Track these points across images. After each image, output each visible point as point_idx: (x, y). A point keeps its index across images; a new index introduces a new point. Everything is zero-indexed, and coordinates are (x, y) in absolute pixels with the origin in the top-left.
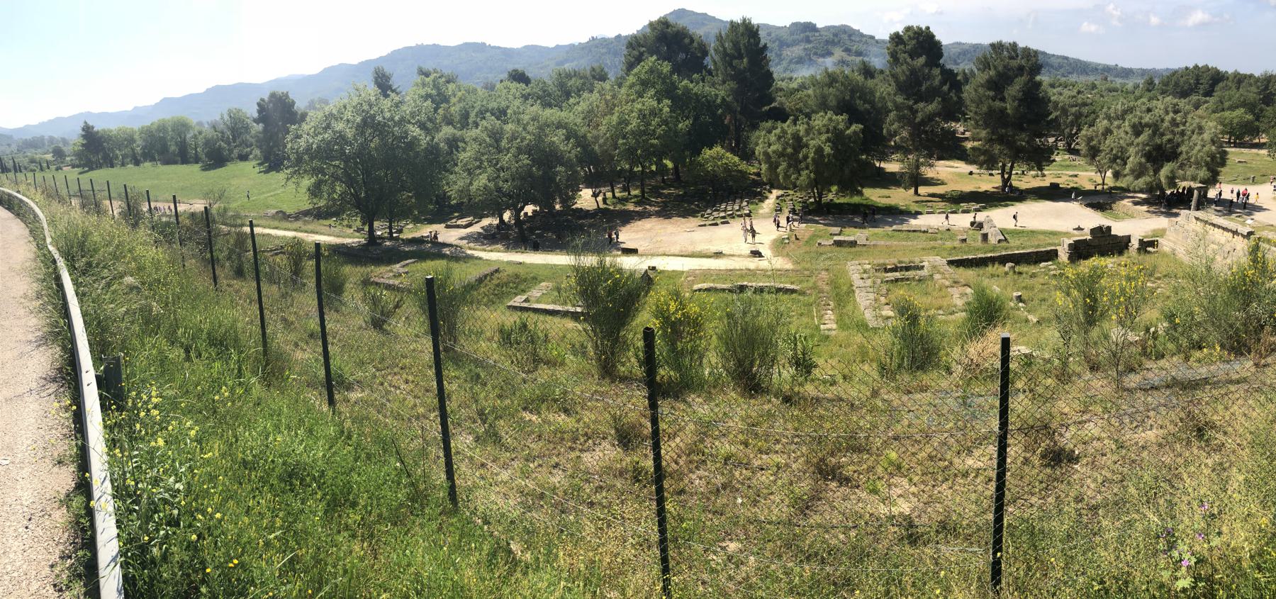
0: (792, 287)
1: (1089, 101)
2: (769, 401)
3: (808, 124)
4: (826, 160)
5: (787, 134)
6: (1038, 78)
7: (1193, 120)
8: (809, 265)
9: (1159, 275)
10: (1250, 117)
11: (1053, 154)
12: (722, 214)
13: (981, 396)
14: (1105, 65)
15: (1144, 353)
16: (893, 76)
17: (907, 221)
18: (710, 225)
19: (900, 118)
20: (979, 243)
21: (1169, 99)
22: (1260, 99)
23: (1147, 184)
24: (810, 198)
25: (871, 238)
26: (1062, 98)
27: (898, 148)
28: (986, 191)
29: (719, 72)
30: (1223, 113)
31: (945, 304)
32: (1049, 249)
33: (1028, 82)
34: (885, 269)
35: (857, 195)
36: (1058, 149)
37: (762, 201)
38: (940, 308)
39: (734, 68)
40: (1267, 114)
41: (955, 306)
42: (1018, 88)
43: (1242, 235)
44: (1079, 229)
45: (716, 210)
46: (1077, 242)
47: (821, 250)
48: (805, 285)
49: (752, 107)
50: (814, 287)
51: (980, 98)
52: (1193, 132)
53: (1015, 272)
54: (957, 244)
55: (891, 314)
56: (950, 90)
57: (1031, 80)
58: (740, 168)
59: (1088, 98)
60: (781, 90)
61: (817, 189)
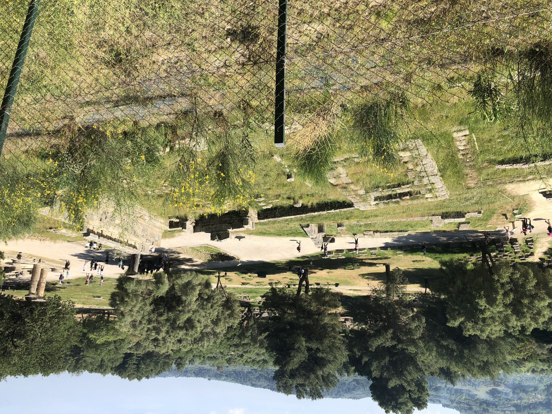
0: (504, 167)
1: (233, 349)
3: (508, 327)
4: (482, 293)
6: (277, 368)
7: (140, 334)
10: (91, 336)
13: (313, 88)
14: (220, 380)
15: (174, 129)
16: (420, 370)
17: (395, 241)
21: (163, 351)
22: (83, 351)
23: (180, 277)
24: (495, 256)
25: (427, 222)
26: (256, 351)
27: (410, 305)
28: (322, 270)
31: (353, 168)
32: (266, 220)
33: (285, 365)
34: (411, 195)
35: (446, 262)
36: (259, 307)
38: (358, 163)
40: (76, 339)
41: (344, 166)
42: (295, 359)
43: (93, 232)
44: (239, 238)
47: (477, 207)
48: (490, 171)
50: (480, 170)
51: (331, 351)
52: (140, 322)
53: (294, 199)
54: (346, 222)
56: (361, 357)
57: (283, 366)
59: (234, 351)
61: (488, 265)
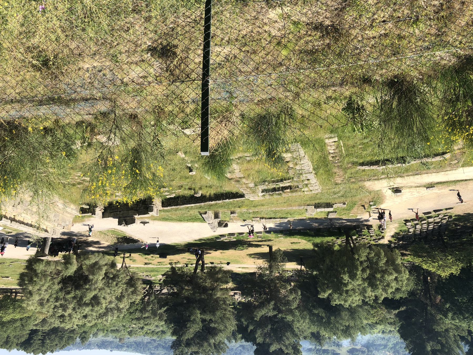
0: (364, 168)
1: (134, 322)
2: (381, 75)
3: (365, 297)
4: (346, 269)
5: (383, 289)
6: (174, 338)
7: (47, 310)
8: (352, 186)
9: (79, 186)
11: (164, 280)
12: (430, 220)
17: (277, 226)
18: (441, 210)
19: (288, 303)
20: (221, 211)
21: (68, 326)
23: (88, 258)
24: (356, 239)
26: (156, 323)
27: (288, 280)
28: (216, 251)
29: (453, 339)
30: (22, 317)
31: (245, 165)
32: (169, 208)
34: (291, 189)
36: (160, 284)
37: (397, 234)
38: (249, 161)
39: (439, 342)
42: (191, 330)
43: (6, 217)
44: (144, 223)
45: (438, 223)
46: (146, 213)
47: (343, 199)
49: (417, 309)
50: (345, 169)
52: (48, 300)
53: (194, 190)
54: (238, 210)
55: (284, 155)
56: (247, 326)
57: (180, 336)
58: (421, 259)
59: (135, 324)
60: (390, 324)
61: (351, 246)
